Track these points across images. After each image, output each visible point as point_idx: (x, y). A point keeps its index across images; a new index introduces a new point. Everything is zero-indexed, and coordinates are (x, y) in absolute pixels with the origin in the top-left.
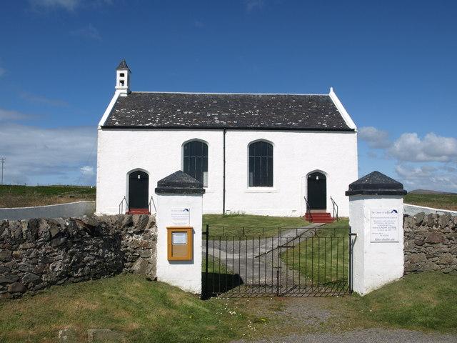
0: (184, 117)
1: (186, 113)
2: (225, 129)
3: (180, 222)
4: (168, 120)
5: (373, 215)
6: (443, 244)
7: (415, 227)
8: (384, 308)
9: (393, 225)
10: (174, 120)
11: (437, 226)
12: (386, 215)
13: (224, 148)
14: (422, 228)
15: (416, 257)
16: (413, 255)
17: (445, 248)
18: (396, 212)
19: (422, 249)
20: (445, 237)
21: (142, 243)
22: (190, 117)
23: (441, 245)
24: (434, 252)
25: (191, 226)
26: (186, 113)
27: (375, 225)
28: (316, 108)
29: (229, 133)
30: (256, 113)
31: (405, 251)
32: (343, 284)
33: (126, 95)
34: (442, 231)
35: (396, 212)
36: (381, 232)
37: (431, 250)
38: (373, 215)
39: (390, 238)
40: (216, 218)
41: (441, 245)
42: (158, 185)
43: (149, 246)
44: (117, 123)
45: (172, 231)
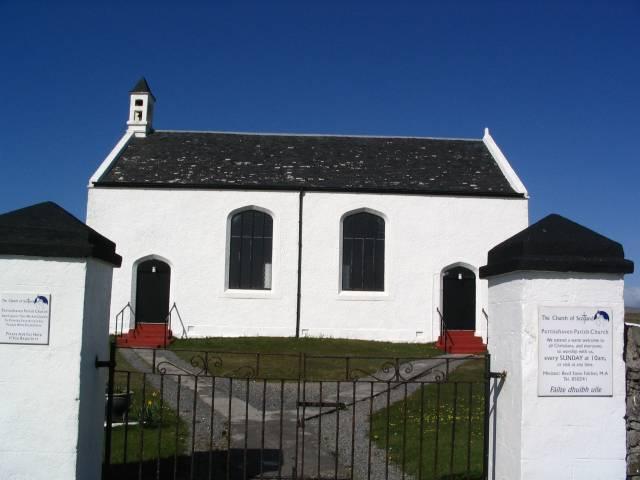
0: (235, 170)
1: (240, 163)
9: (597, 352)
12: (580, 325)
26: (240, 163)
27: (553, 352)
29: (309, 196)
30: (356, 165)
33: (144, 136)
36: (567, 369)
44: (121, 178)
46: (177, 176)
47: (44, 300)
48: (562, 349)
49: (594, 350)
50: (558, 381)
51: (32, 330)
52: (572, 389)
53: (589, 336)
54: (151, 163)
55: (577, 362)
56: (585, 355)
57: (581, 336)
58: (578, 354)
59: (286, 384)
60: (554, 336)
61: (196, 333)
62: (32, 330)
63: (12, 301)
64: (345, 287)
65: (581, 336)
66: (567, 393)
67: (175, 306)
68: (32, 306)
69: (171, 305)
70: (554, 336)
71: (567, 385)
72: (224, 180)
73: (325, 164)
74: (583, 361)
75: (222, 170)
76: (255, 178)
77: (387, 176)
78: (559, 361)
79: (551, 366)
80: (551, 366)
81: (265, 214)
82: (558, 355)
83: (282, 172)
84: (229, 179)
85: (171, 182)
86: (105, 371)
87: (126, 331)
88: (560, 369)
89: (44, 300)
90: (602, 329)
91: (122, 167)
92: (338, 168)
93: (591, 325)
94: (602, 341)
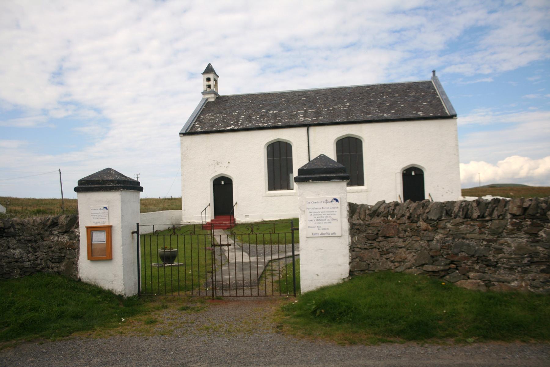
0: (268, 117)
1: (271, 112)
2: (308, 126)
3: (99, 220)
4: (250, 122)
5: (309, 206)
6: (399, 238)
7: (368, 218)
8: (328, 310)
9: (333, 217)
10: (257, 121)
11: (393, 216)
12: (325, 205)
13: (309, 147)
14: (377, 220)
15: (367, 254)
16: (363, 251)
17: (400, 243)
18: (337, 200)
19: (375, 244)
20: (400, 229)
21: (67, 243)
22: (274, 116)
23: (396, 239)
24: (388, 248)
25: (111, 225)
26: (271, 112)
27: (312, 218)
28: (414, 96)
29: (312, 130)
30: (345, 106)
31: (352, 249)
32: (293, 283)
33: (213, 100)
34: (398, 222)
35: (337, 200)
36: (319, 225)
37: (385, 245)
38: (309, 206)
39: (331, 231)
40: (449, 213)
41: (396, 239)
42: (78, 184)
43: (74, 248)
44: (199, 129)
45: (91, 230)
46: (232, 124)
47: (106, 208)
48: (316, 216)
49: (332, 216)
50: (316, 230)
51: (103, 220)
52: (322, 234)
53: (328, 210)
54: (218, 117)
55: (324, 221)
56: (327, 218)
57: (326, 210)
58: (324, 218)
59: (265, 246)
60: (312, 211)
61: (254, 218)
62: (103, 220)
63: (314, 203)
64: (270, 189)
65: (326, 210)
66: (319, 236)
67: (236, 203)
68: (102, 211)
69: (234, 203)
70: (312, 211)
71: (319, 232)
72: (261, 124)
73: (324, 108)
74: (327, 221)
75: (260, 118)
76: (279, 121)
77: (363, 112)
78: (315, 221)
79: (312, 224)
80: (312, 224)
81: (287, 143)
82: (315, 219)
83: (297, 115)
84: (264, 123)
85: (229, 128)
86: (135, 235)
87: (209, 220)
88: (316, 225)
89: (106, 208)
90: (335, 206)
91: (200, 122)
92: (332, 110)
93: (330, 205)
94: (336, 212)
